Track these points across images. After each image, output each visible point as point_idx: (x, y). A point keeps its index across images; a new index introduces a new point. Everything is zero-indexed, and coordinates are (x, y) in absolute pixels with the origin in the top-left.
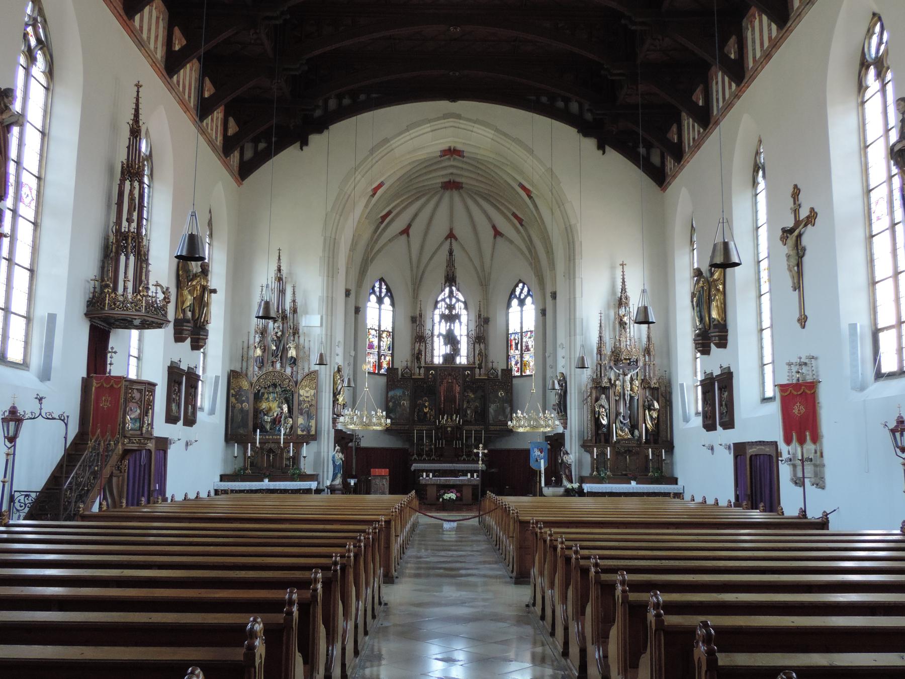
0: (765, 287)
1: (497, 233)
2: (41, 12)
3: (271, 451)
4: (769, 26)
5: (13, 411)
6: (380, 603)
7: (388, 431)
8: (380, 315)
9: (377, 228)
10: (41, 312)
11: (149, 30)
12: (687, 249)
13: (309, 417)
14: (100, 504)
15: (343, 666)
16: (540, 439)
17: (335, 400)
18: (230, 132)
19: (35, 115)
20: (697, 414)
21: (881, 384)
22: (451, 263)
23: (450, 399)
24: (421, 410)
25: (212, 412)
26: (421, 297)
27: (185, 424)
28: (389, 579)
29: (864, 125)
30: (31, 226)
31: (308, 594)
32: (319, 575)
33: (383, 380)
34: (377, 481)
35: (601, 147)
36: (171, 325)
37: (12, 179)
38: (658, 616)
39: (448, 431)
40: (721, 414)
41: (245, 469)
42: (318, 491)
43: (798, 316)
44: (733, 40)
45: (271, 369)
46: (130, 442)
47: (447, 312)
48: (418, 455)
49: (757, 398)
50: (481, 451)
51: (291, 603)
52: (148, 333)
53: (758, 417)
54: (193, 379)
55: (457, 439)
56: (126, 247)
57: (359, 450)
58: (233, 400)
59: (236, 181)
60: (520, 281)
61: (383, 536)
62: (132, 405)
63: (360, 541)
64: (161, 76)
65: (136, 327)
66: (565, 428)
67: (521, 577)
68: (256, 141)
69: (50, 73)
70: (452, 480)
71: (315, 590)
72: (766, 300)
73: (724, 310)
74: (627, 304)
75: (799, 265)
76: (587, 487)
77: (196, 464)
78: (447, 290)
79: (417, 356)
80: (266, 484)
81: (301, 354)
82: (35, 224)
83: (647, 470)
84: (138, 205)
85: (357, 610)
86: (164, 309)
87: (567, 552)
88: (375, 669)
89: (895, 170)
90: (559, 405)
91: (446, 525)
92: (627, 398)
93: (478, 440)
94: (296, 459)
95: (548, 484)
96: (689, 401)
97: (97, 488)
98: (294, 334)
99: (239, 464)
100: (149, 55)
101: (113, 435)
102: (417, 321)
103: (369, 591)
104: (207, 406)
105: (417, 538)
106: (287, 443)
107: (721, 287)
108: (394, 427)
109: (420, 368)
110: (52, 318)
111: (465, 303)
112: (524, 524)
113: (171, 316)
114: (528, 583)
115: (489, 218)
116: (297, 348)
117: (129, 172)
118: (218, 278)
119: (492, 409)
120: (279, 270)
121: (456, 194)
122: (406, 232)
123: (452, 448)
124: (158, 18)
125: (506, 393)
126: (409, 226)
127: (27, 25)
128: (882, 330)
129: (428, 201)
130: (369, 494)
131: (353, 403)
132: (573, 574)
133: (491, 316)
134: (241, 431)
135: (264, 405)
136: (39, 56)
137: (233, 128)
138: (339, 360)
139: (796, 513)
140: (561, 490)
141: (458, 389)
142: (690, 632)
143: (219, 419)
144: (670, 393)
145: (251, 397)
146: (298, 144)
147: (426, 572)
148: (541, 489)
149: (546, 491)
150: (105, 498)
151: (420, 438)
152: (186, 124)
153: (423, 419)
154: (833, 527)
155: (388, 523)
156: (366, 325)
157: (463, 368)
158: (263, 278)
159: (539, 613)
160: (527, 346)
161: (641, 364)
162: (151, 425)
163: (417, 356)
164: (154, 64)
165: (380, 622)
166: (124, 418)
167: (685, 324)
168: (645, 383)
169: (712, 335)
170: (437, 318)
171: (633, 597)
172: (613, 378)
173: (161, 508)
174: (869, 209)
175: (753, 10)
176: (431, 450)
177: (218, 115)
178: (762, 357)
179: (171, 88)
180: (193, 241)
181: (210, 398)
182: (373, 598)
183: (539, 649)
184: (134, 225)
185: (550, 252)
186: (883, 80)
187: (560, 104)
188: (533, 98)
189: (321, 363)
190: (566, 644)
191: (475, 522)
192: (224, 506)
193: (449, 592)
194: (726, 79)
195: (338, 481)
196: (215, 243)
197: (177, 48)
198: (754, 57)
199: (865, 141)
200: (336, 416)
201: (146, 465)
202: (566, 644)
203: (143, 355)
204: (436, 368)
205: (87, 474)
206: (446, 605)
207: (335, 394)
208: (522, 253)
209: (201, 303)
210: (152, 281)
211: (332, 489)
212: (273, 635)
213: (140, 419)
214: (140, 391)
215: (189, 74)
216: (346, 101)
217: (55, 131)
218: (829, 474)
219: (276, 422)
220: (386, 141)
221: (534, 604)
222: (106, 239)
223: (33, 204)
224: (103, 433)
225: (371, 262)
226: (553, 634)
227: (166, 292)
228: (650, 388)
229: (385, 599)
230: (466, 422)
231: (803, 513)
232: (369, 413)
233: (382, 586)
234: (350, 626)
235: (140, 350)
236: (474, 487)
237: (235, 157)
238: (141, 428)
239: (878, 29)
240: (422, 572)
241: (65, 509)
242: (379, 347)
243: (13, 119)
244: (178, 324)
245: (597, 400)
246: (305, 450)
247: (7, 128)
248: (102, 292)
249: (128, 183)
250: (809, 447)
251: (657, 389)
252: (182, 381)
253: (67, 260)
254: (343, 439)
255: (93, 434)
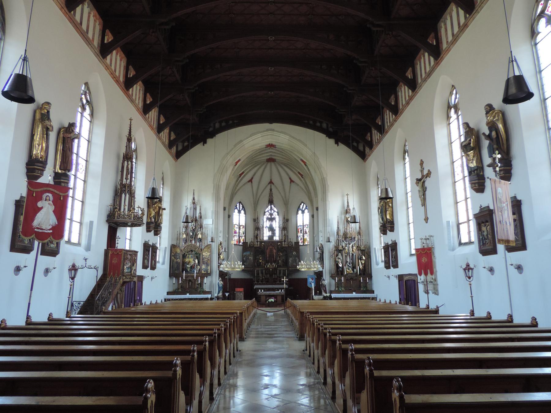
0: (410, 205)
1: (292, 181)
2: (88, 89)
3: (190, 281)
4: (408, 91)
5: (74, 266)
6: (237, 350)
7: (243, 271)
8: (239, 218)
9: (238, 179)
10: (86, 220)
11: (136, 95)
12: (376, 187)
13: (207, 265)
14: (112, 307)
15: (219, 379)
16: (312, 274)
17: (219, 257)
18: (172, 138)
19: (85, 133)
20: (382, 261)
21: (462, 247)
22: (271, 195)
23: (271, 256)
24: (258, 261)
25: (163, 263)
26: (258, 210)
27: (151, 269)
28: (242, 339)
29: (450, 133)
30: (83, 182)
31: (202, 347)
32: (207, 339)
33: (241, 248)
34: (238, 294)
35: (337, 143)
36: (145, 225)
37: (74, 162)
38: (352, 355)
39: (271, 270)
40: (392, 261)
41: (178, 289)
42: (212, 299)
43: (424, 217)
44: (393, 97)
45: (190, 243)
46: (126, 278)
47: (269, 217)
48: (258, 281)
49: (408, 254)
50: (285, 280)
51: (194, 351)
52: (135, 229)
53: (408, 264)
54: (154, 249)
55: (275, 274)
56: (125, 191)
57: (231, 280)
58: (173, 258)
59: (175, 159)
60: (302, 202)
61: (238, 320)
62: (127, 261)
63: (227, 322)
64: (141, 115)
65: (129, 226)
66: (323, 268)
67: (301, 338)
68: (183, 142)
69: (92, 115)
70: (272, 293)
71: (205, 345)
72: (410, 210)
73: (392, 215)
74: (349, 212)
75: (424, 195)
76: (333, 295)
77: (156, 288)
78: (269, 207)
79: (256, 237)
80: (188, 296)
81: (204, 237)
82: (85, 181)
83: (360, 287)
84: (130, 172)
85: (226, 353)
86: (142, 217)
87: (319, 326)
88: (235, 380)
89: (463, 154)
90: (320, 258)
91: (269, 314)
92: (351, 255)
93: (284, 275)
94: (201, 284)
95: (316, 294)
96: (378, 256)
97: (110, 300)
98: (200, 228)
99: (176, 287)
100: (136, 106)
101: (118, 275)
102: (256, 221)
103: (232, 345)
104: (161, 261)
105: (256, 320)
106: (197, 277)
107: (391, 205)
108: (246, 269)
109: (257, 242)
110: (91, 223)
111: (278, 212)
112: (302, 313)
113: (145, 221)
114: (304, 340)
115: (288, 174)
116: (202, 234)
117: (127, 158)
118: (166, 203)
119: (290, 260)
120: (194, 199)
121: (273, 164)
122: (251, 181)
123: (272, 278)
124: (140, 90)
125: (297, 253)
126: (252, 178)
127: (82, 94)
128: (461, 223)
129: (261, 166)
130: (235, 300)
131: (228, 258)
132: (321, 336)
133: (289, 218)
134: (176, 272)
135: (187, 260)
136: (87, 108)
137: (173, 137)
138: (221, 239)
139: (425, 307)
140: (321, 297)
141: (275, 251)
142: (363, 361)
143: (167, 267)
144: (370, 252)
145: (181, 256)
146: (202, 143)
147: (259, 335)
148: (312, 296)
149: (315, 297)
150: (114, 304)
151: (258, 274)
152: (152, 135)
153: (259, 265)
154: (441, 313)
155: (241, 314)
156: (233, 223)
157: (277, 242)
158: (187, 203)
159: (308, 354)
160: (306, 232)
161: (356, 239)
162: (135, 270)
163: (256, 237)
164: (138, 110)
165: (238, 359)
166: (123, 267)
167: (376, 222)
168: (358, 248)
169: (388, 226)
170: (265, 219)
171: (344, 346)
172: (344, 246)
173: (140, 308)
174: (454, 170)
175: (401, 83)
176: (263, 279)
177: (167, 131)
178: (409, 236)
179: (145, 120)
180: (154, 190)
181: (162, 257)
182: (234, 348)
183: (309, 370)
184: (129, 181)
185: (315, 189)
186: (457, 114)
187: (318, 124)
188: (306, 122)
189: (212, 242)
190: (319, 368)
191: (282, 312)
192: (169, 307)
193: (270, 345)
194: (391, 113)
195: (220, 294)
196: (165, 187)
197: (148, 102)
198: (402, 104)
199: (451, 140)
200: (220, 264)
201: (134, 288)
202: (319, 368)
203: (131, 239)
204: (265, 242)
205: (107, 293)
206: (268, 351)
207: (219, 255)
208: (303, 189)
209: (158, 215)
210: (136, 206)
211: (218, 298)
212: (186, 366)
213: (131, 268)
214: (130, 255)
215: (153, 114)
216: (223, 124)
217: (94, 140)
218: (440, 288)
219: (192, 267)
220: (241, 141)
221: (306, 350)
222: (116, 187)
223: (84, 172)
224: (114, 275)
225: (235, 194)
226: (313, 363)
227: (143, 210)
228: (361, 250)
229: (240, 348)
230: (279, 266)
231: (428, 307)
232: (234, 263)
233: (239, 343)
234: (222, 361)
235: (131, 236)
236: (282, 296)
237: (174, 150)
238: (131, 272)
239: (454, 92)
240: (259, 335)
241: (96, 309)
242: (239, 233)
243: (75, 136)
244: (148, 224)
245: (337, 255)
246: (205, 280)
247: (73, 140)
248: (114, 211)
249: (126, 162)
250: (429, 277)
251: (364, 250)
252: (150, 250)
253: (98, 198)
254: (222, 275)
255: (109, 275)
